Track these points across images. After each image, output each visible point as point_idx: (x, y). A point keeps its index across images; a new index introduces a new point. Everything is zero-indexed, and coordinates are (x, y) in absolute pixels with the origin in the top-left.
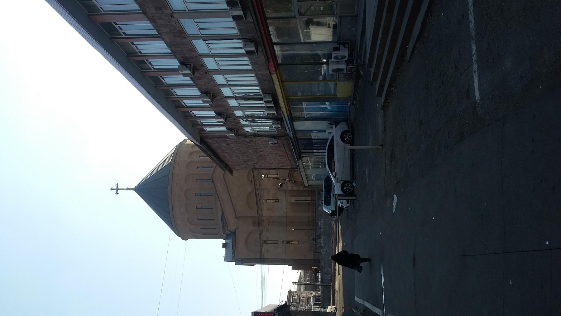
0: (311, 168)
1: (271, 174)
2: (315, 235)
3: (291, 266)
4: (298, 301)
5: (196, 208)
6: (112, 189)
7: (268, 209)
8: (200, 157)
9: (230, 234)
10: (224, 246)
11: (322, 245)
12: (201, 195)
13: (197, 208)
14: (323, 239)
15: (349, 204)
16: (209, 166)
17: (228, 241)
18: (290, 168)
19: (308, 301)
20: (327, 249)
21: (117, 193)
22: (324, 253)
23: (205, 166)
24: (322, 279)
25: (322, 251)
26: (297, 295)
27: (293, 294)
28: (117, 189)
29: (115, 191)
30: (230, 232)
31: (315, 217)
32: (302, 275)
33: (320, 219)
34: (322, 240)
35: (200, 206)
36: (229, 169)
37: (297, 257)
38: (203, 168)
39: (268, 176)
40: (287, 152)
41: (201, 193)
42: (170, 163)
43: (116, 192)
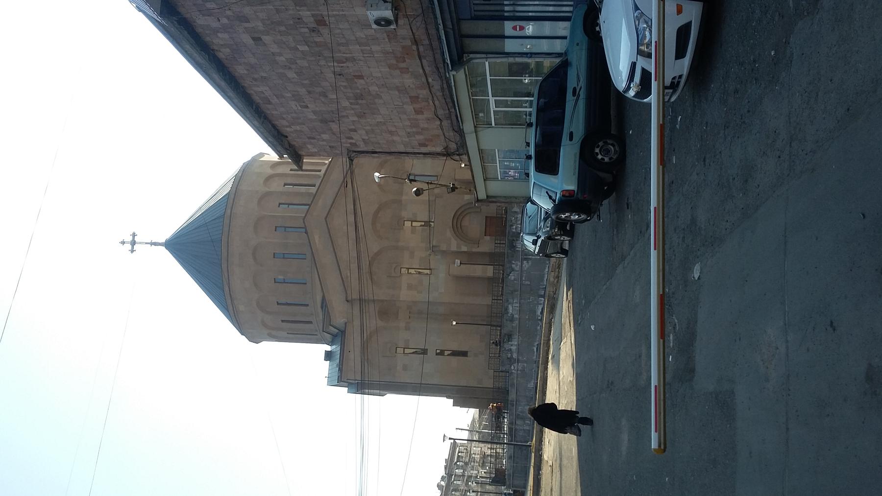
0: (500, 179)
1: (418, 220)
2: (500, 333)
3: (452, 400)
4: (467, 460)
5: (273, 282)
6: (123, 243)
7: (410, 287)
8: (285, 185)
9: (337, 333)
10: (328, 356)
11: (515, 356)
12: (284, 258)
13: (275, 282)
14: (516, 343)
15: (687, 61)
16: (301, 203)
17: (334, 347)
18: (439, 149)
19: (483, 461)
20: (525, 365)
21: (132, 251)
22: (519, 372)
23: (294, 202)
24: (510, 429)
25: (512, 368)
26: (467, 450)
27: (459, 448)
28: (133, 243)
29: (129, 247)
30: (337, 331)
31: (502, 294)
32: (477, 416)
33: (511, 300)
34: (514, 345)
35: (281, 277)
36: (287, 147)
37: (463, 383)
38: (290, 206)
39: (413, 223)
40: (430, 80)
41: (284, 254)
42: (228, 194)
43: (130, 249)
